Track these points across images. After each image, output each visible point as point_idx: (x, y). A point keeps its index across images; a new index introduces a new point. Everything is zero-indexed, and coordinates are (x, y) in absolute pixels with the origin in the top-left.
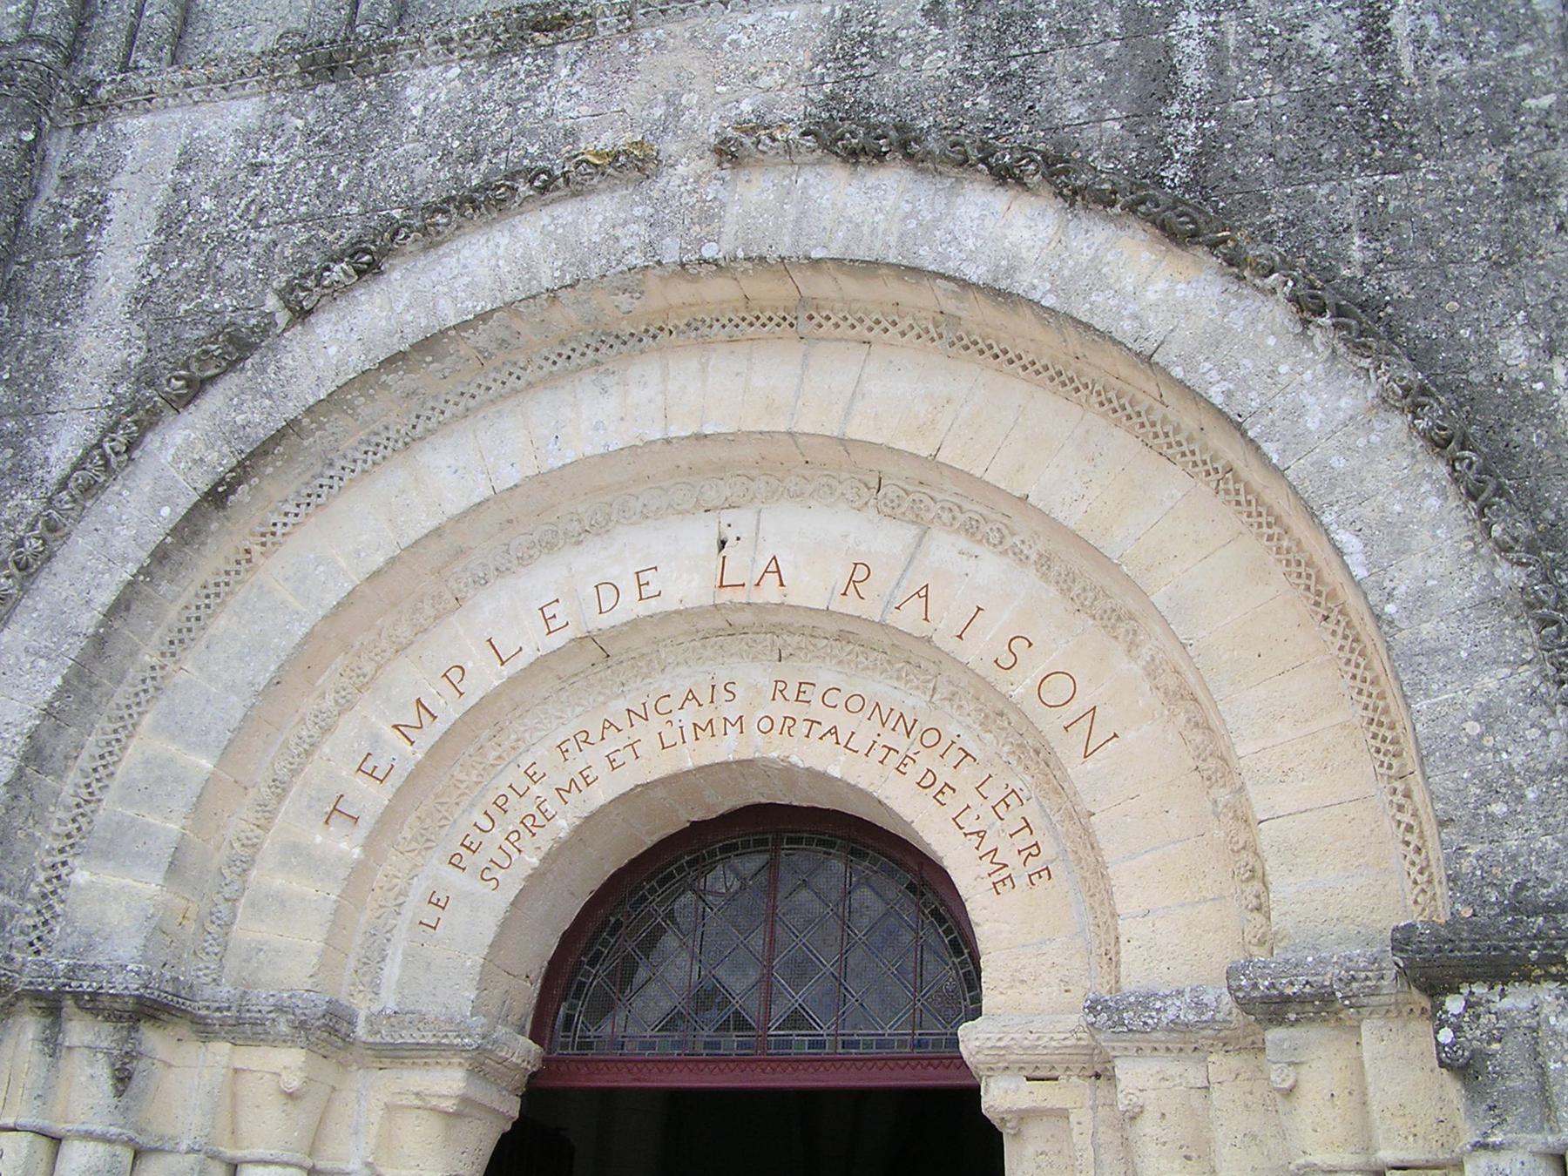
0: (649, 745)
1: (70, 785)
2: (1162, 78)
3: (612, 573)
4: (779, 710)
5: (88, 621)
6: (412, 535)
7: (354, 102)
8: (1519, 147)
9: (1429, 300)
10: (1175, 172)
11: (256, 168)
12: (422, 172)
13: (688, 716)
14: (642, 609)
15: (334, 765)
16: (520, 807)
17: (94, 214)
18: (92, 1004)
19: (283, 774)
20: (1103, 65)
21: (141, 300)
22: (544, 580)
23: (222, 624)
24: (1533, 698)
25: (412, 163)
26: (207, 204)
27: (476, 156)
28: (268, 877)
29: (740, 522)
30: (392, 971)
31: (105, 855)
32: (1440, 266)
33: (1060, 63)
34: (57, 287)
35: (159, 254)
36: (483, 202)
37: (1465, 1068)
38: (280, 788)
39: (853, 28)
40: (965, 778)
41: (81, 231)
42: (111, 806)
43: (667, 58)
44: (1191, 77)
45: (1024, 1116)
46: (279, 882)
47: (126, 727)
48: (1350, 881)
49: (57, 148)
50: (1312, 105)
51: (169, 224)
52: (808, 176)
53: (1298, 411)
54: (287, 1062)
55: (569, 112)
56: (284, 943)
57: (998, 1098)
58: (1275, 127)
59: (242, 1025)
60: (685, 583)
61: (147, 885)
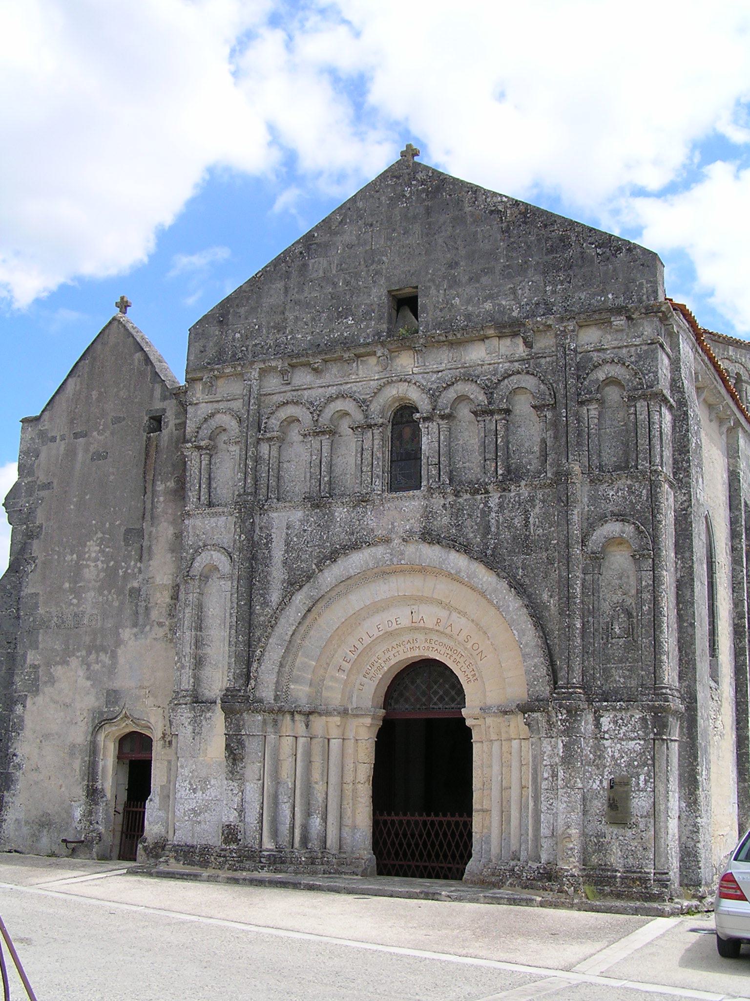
0: (401, 652)
1: (287, 669)
2: (488, 527)
3: (391, 619)
4: (427, 645)
5: (287, 638)
6: (350, 615)
7: (324, 515)
8: (549, 552)
9: (532, 584)
10: (489, 552)
11: (305, 531)
12: (342, 536)
13: (408, 646)
14: (397, 627)
15: (338, 659)
16: (377, 665)
17: (269, 541)
18: (300, 713)
19: (328, 660)
20: (476, 524)
21: (285, 563)
22: (377, 619)
23: (312, 633)
24: (542, 664)
25: (339, 534)
26: (295, 539)
27: (353, 534)
28: (328, 683)
29: (415, 607)
30: (354, 699)
31: (296, 682)
32: (534, 577)
33: (468, 523)
34: (265, 558)
35: (286, 552)
36: (355, 547)
37: (528, 724)
38: (328, 664)
39: (428, 509)
40: (462, 660)
41: (267, 543)
42: (295, 672)
43: (391, 512)
44: (493, 529)
45: (474, 726)
46: (330, 684)
47: (296, 656)
48: (518, 692)
49: (257, 521)
50: (514, 538)
51: (287, 544)
52: (421, 546)
53: (508, 607)
54: (337, 720)
55: (373, 525)
56: (334, 696)
57: (468, 723)
58: (508, 543)
59: (328, 713)
60: (405, 622)
61: (306, 689)
